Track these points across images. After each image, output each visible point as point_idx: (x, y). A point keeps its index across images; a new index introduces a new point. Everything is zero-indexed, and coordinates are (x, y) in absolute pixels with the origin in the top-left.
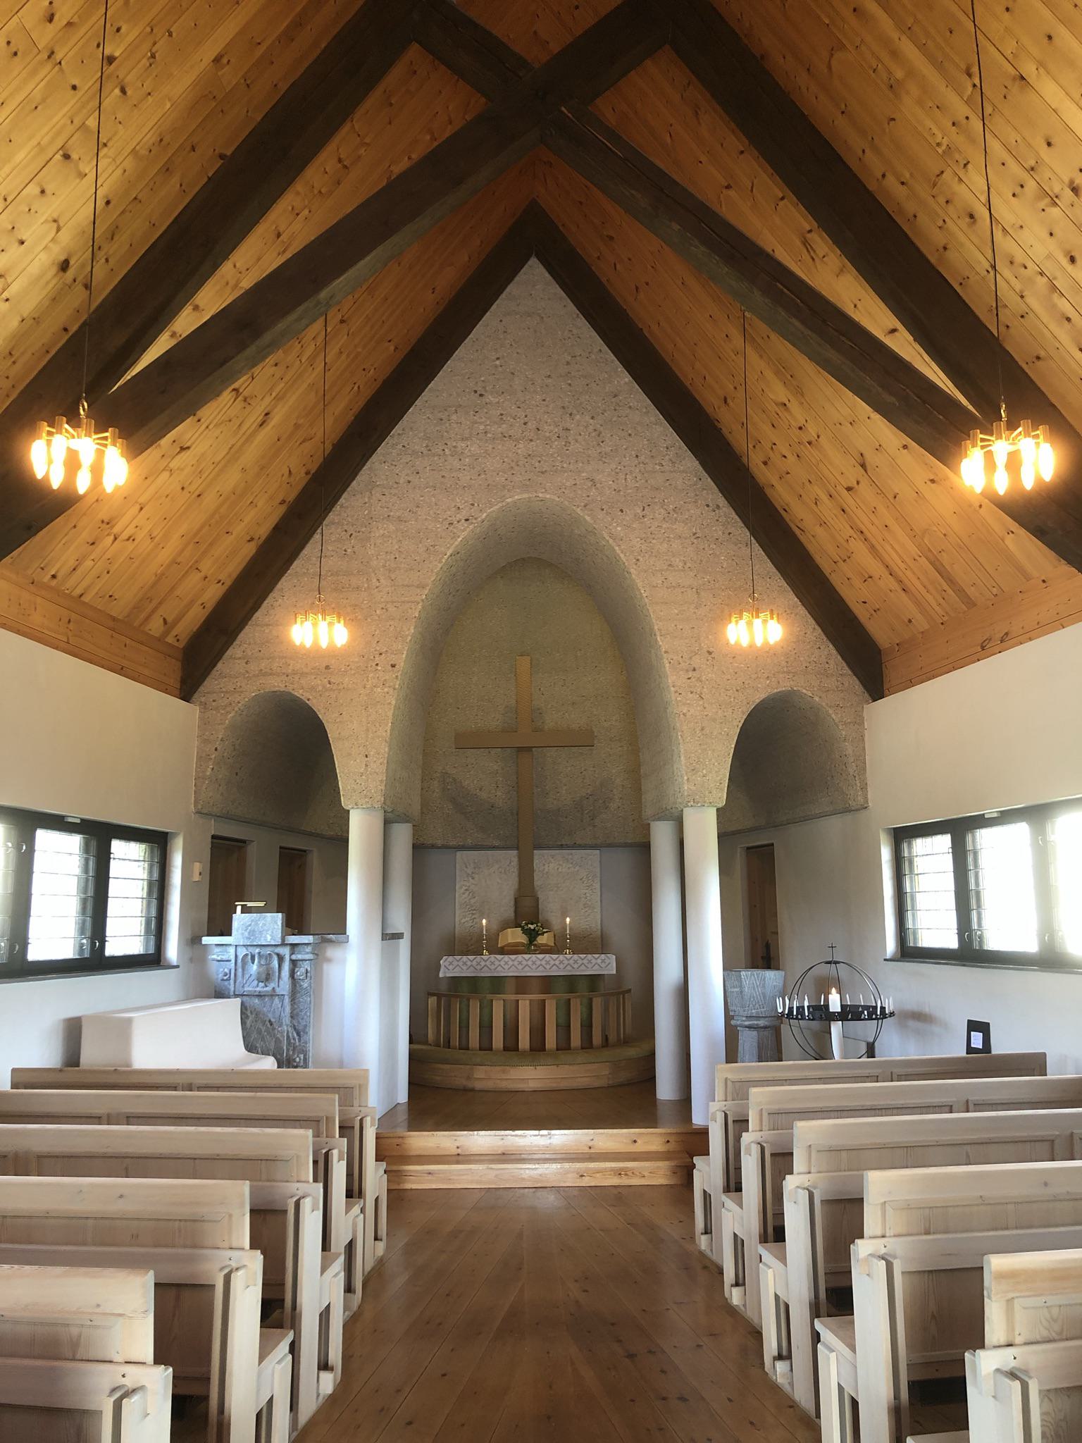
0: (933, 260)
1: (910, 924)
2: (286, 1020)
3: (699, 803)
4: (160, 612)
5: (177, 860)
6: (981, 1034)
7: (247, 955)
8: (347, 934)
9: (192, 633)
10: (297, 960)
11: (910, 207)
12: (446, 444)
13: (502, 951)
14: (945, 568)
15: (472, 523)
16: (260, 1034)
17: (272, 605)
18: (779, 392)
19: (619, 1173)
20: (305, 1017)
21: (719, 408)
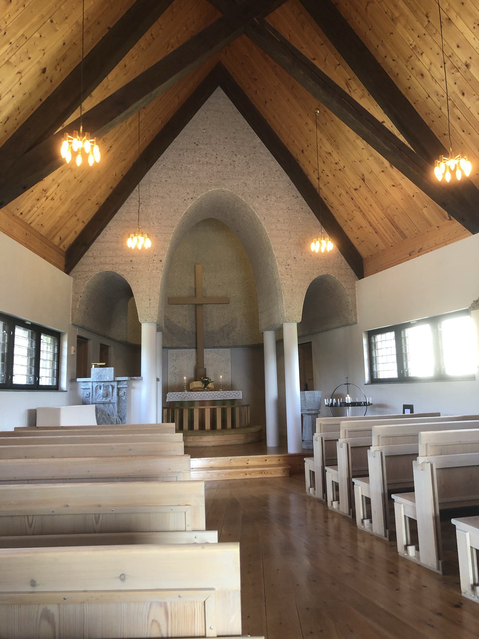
0: (404, 93)
1: (375, 370)
2: (116, 413)
3: (290, 321)
4: (59, 234)
5: (65, 345)
6: (410, 410)
7: (97, 386)
8: (142, 376)
9: (70, 245)
10: (120, 388)
11: (396, 70)
12: (182, 165)
13: (192, 391)
14: (396, 223)
15: (194, 200)
16: (104, 420)
17: (105, 234)
18: (328, 147)
19: (261, 472)
20: (124, 412)
21: (299, 155)
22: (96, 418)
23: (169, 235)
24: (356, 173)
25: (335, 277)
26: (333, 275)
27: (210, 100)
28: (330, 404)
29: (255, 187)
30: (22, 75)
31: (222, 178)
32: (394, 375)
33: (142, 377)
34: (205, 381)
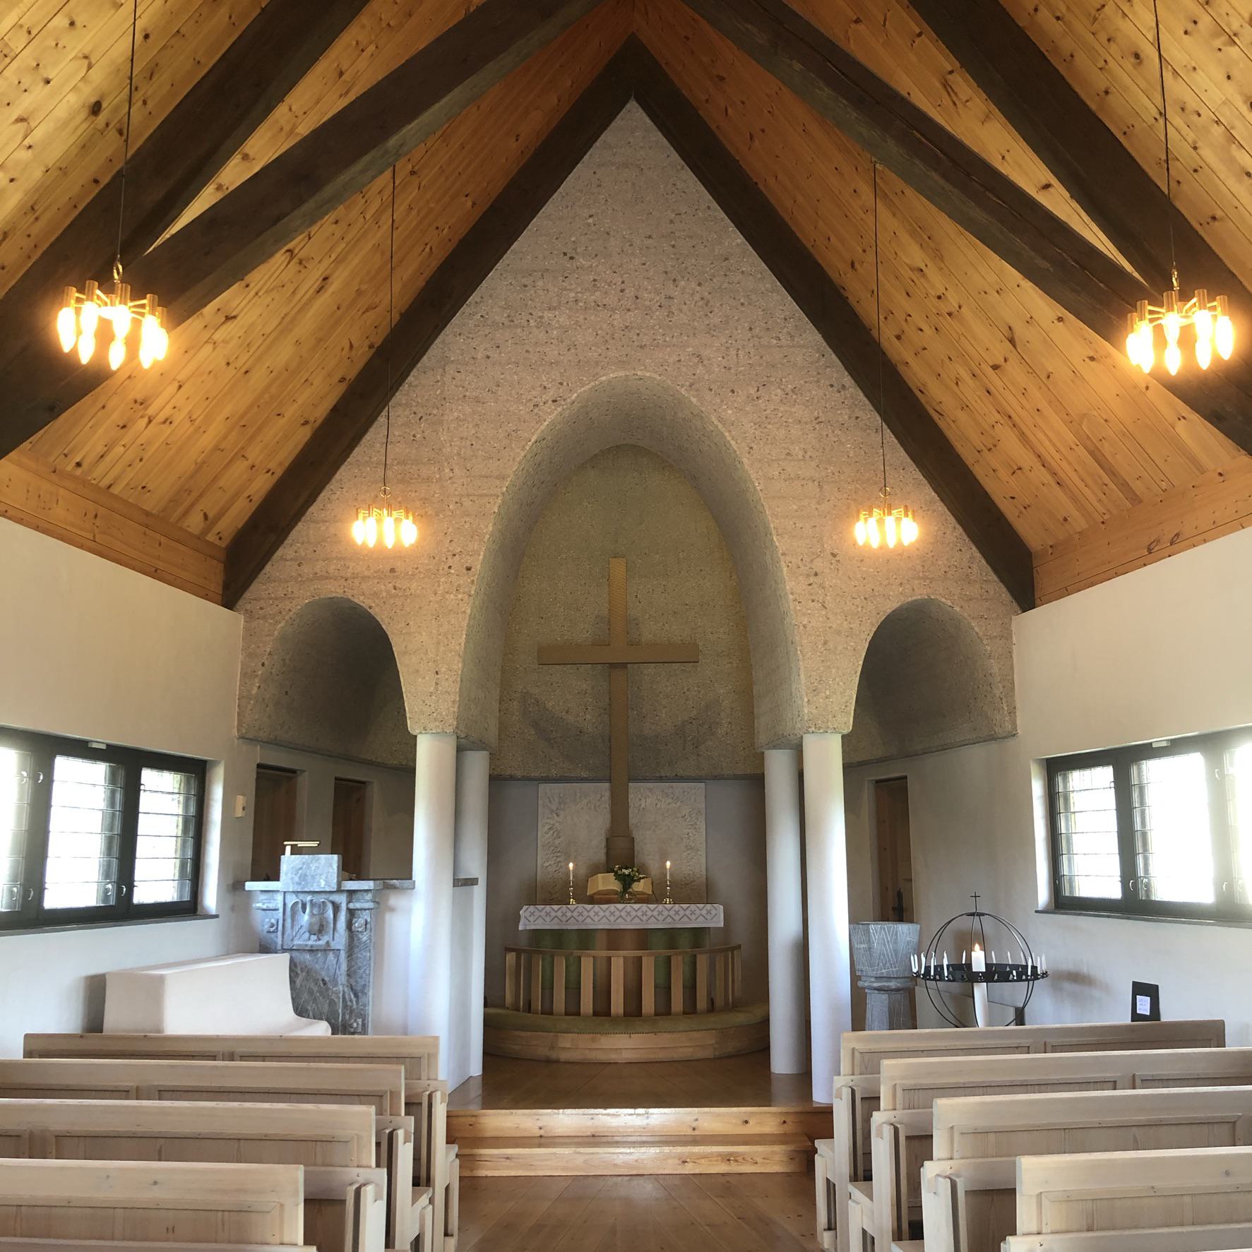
1: (1065, 870)
2: (342, 979)
7: (296, 903)
10: (355, 910)
11: (1067, 45)
12: (532, 314)
17: (329, 499)
18: (915, 255)
19: (728, 1158)
20: (364, 975)
22: (291, 989)
23: (491, 501)
24: (992, 323)
25: (950, 604)
26: (946, 599)
27: (607, 136)
28: (923, 972)
29: (725, 364)
30: (31, 124)
31: (636, 344)
32: (1112, 890)
33: (414, 881)
34: (624, 874)
